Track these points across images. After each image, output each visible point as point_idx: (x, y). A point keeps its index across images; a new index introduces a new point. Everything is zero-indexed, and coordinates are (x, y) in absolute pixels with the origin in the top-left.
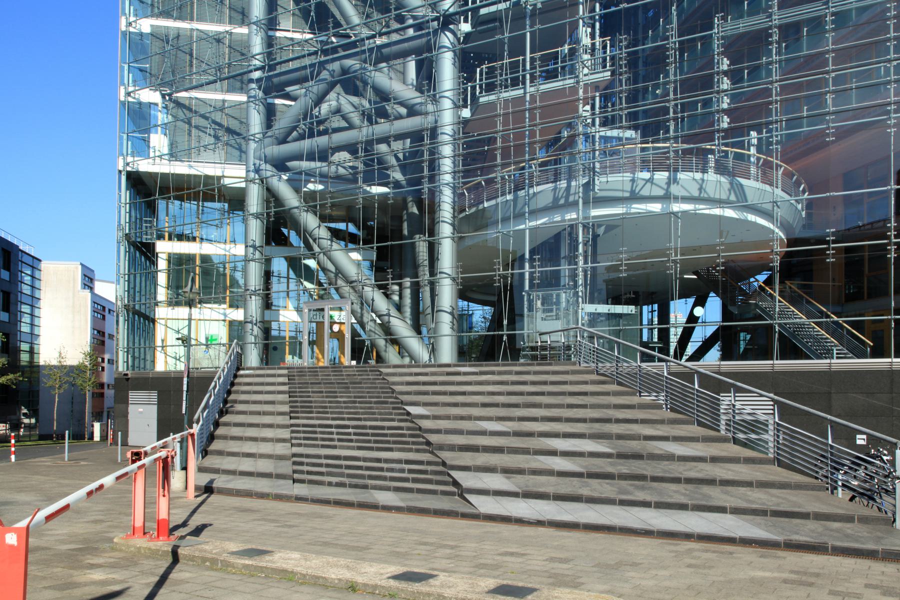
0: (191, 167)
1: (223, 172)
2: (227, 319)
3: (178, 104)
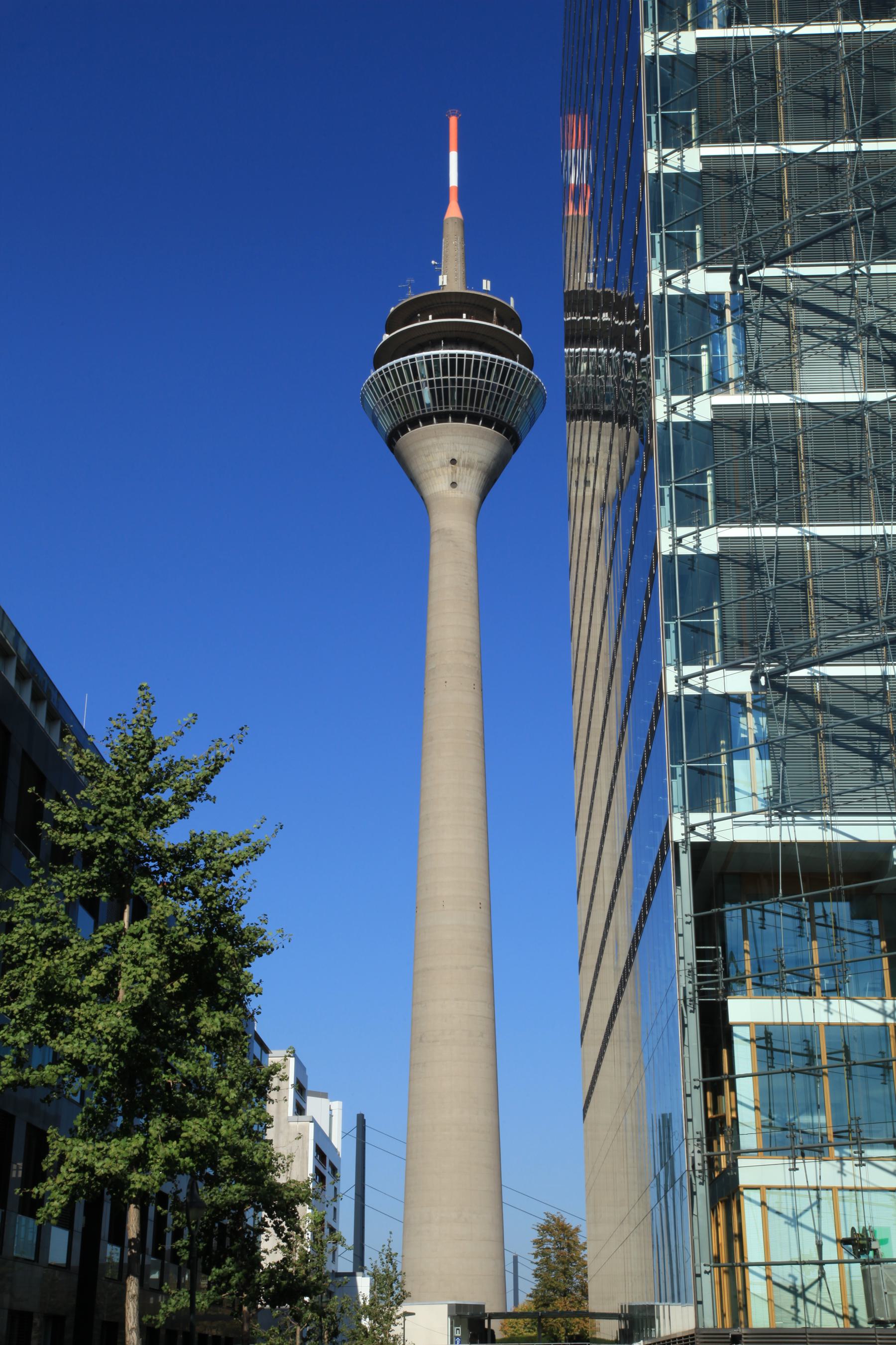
0: (826, 825)
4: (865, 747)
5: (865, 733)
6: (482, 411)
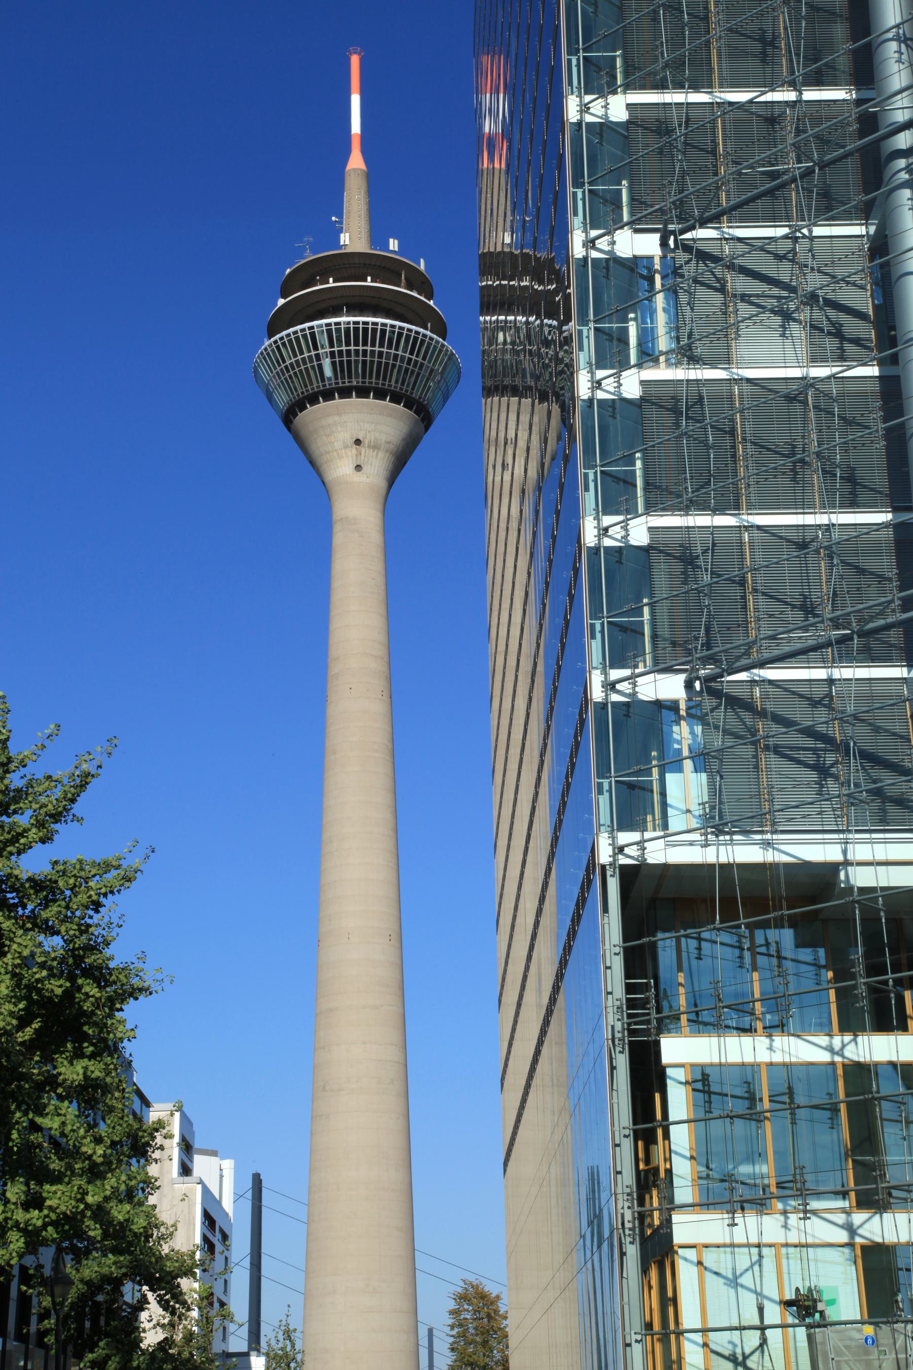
0: (767, 844)
1: (845, 852)
2: (858, 1240)
3: (734, 702)
4: (810, 758)
5: (810, 743)
6: (390, 386)
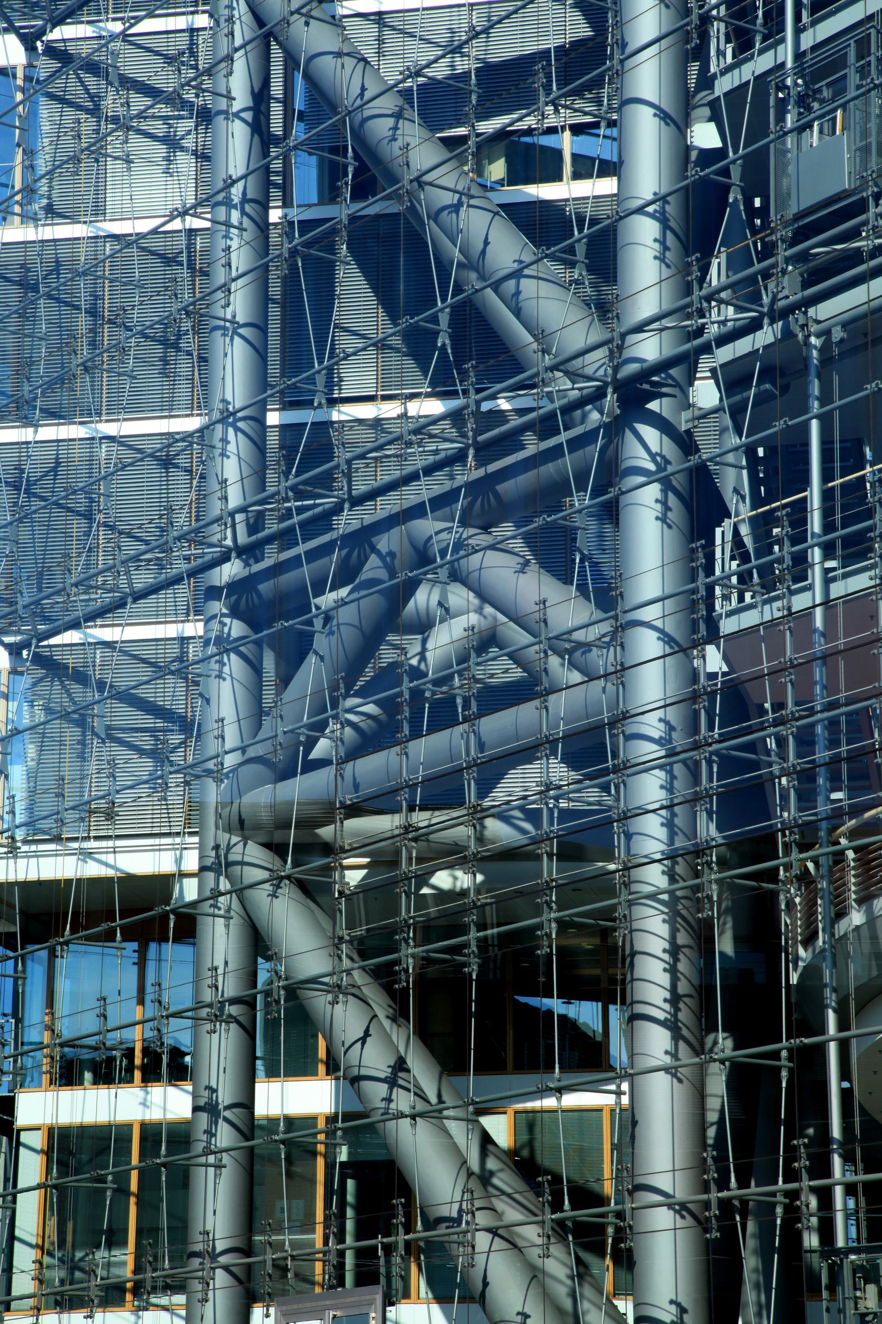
0: (86, 855)
4: (145, 741)
5: (149, 721)
